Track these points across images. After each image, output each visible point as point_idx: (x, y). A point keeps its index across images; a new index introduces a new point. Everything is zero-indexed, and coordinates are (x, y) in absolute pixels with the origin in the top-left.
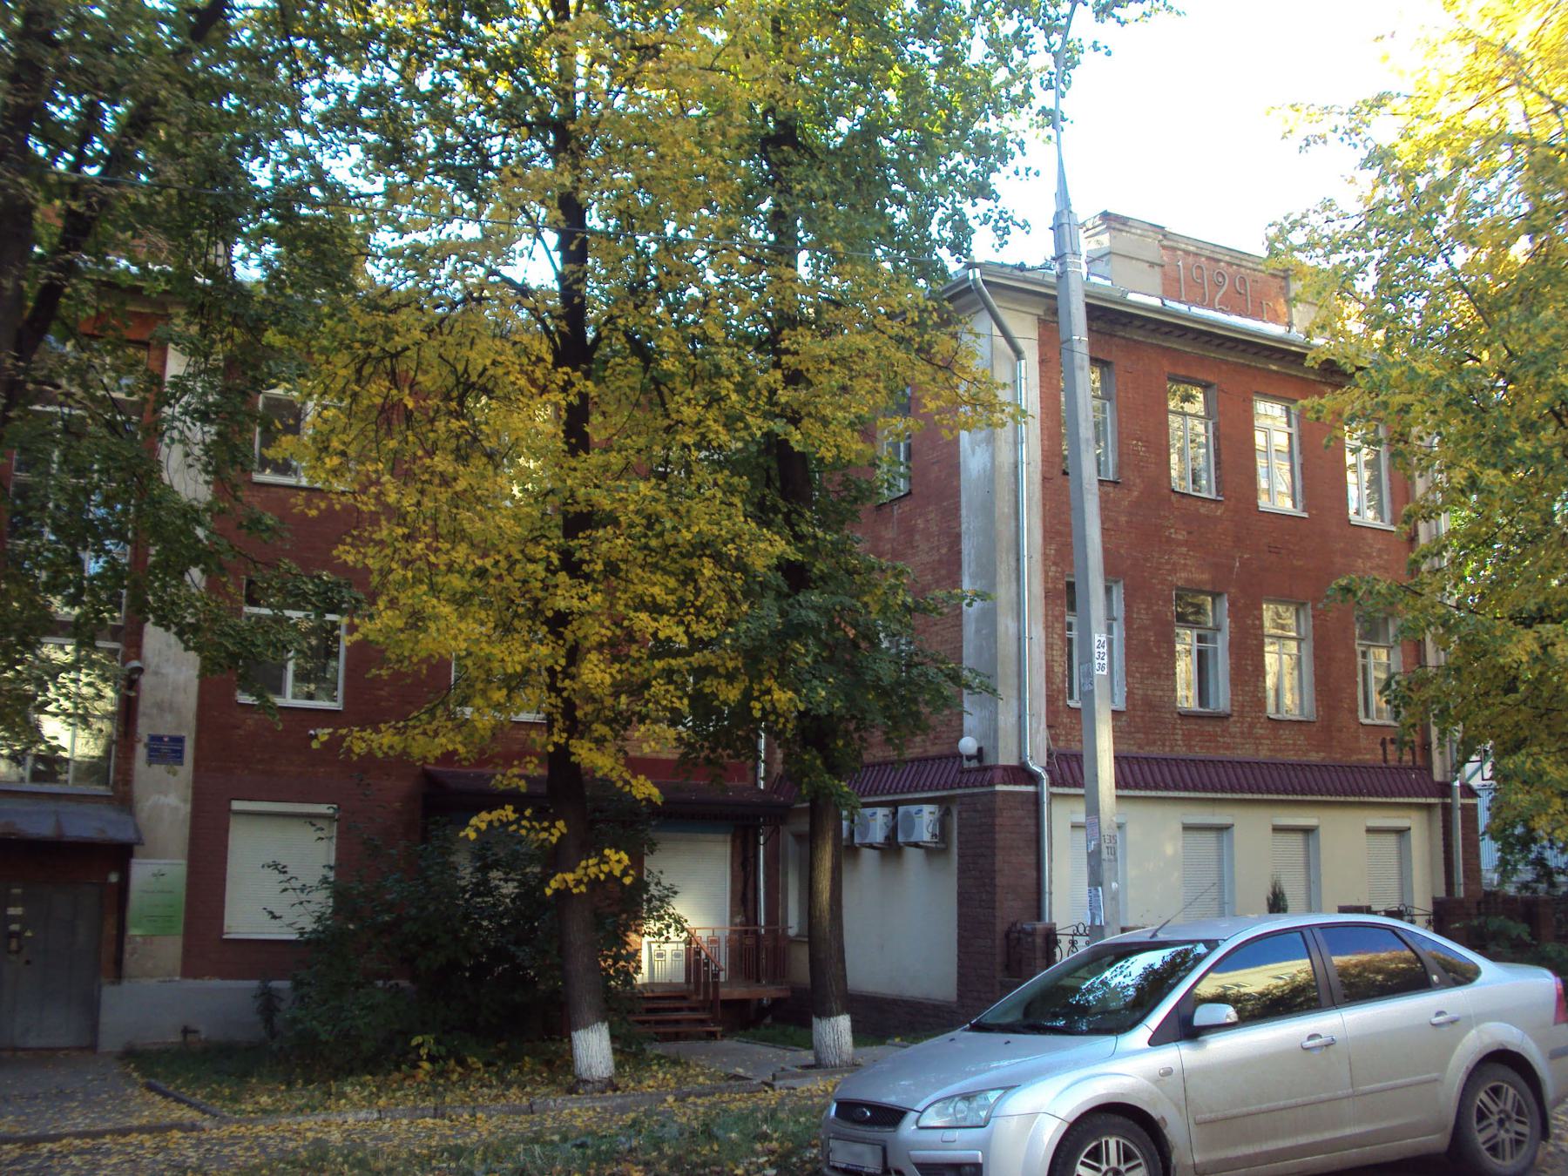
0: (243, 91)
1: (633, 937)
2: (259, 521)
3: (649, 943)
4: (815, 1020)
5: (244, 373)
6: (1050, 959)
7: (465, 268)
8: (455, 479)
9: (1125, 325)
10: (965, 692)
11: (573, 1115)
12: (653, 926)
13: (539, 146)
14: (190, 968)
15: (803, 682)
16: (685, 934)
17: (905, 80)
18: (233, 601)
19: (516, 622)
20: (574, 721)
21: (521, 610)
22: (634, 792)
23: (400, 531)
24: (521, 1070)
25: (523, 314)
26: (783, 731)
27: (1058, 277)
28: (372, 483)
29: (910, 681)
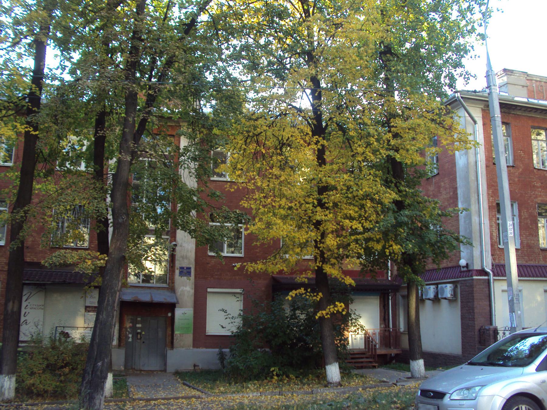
0: (203, 50)
1: (346, 333)
2: (215, 194)
4: (411, 361)
5: (207, 144)
6: (496, 339)
7: (280, 104)
8: (280, 177)
9: (514, 109)
10: (461, 244)
11: (327, 395)
12: (353, 329)
13: (302, 60)
15: (403, 242)
16: (364, 332)
17: (428, 28)
18: (207, 221)
19: (303, 225)
20: (324, 258)
21: (305, 220)
22: (346, 282)
23: (262, 195)
25: (300, 119)
26: (397, 260)
27: (489, 94)
28: (252, 179)
29: (441, 241)
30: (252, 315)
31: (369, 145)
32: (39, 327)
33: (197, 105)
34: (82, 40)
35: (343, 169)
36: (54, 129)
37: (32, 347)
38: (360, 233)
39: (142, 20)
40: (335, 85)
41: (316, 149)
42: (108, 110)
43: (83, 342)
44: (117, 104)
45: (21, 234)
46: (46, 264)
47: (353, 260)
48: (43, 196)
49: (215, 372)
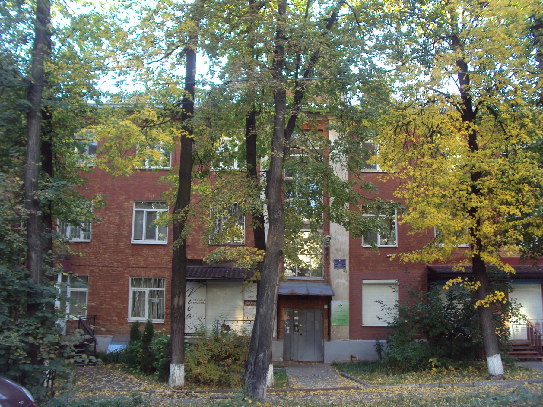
0: (346, 44)
1: (506, 323)
2: (368, 185)
3: (512, 325)
5: (358, 136)
8: (432, 165)
11: (489, 388)
12: (514, 319)
14: (353, 335)
19: (458, 213)
21: (459, 208)
22: (505, 270)
23: (415, 184)
24: (468, 371)
25: (449, 104)
30: (408, 306)
31: (523, 126)
32: (202, 320)
33: (344, 99)
34: (228, 44)
35: (497, 153)
36: (208, 132)
37: (198, 339)
38: (518, 219)
39: (284, 19)
40: (483, 67)
41: (468, 134)
42: (257, 110)
43: (244, 335)
44: (266, 103)
45: (183, 233)
46: (208, 261)
47: (512, 246)
48: (201, 196)
49: (372, 363)
